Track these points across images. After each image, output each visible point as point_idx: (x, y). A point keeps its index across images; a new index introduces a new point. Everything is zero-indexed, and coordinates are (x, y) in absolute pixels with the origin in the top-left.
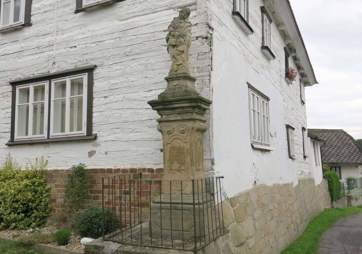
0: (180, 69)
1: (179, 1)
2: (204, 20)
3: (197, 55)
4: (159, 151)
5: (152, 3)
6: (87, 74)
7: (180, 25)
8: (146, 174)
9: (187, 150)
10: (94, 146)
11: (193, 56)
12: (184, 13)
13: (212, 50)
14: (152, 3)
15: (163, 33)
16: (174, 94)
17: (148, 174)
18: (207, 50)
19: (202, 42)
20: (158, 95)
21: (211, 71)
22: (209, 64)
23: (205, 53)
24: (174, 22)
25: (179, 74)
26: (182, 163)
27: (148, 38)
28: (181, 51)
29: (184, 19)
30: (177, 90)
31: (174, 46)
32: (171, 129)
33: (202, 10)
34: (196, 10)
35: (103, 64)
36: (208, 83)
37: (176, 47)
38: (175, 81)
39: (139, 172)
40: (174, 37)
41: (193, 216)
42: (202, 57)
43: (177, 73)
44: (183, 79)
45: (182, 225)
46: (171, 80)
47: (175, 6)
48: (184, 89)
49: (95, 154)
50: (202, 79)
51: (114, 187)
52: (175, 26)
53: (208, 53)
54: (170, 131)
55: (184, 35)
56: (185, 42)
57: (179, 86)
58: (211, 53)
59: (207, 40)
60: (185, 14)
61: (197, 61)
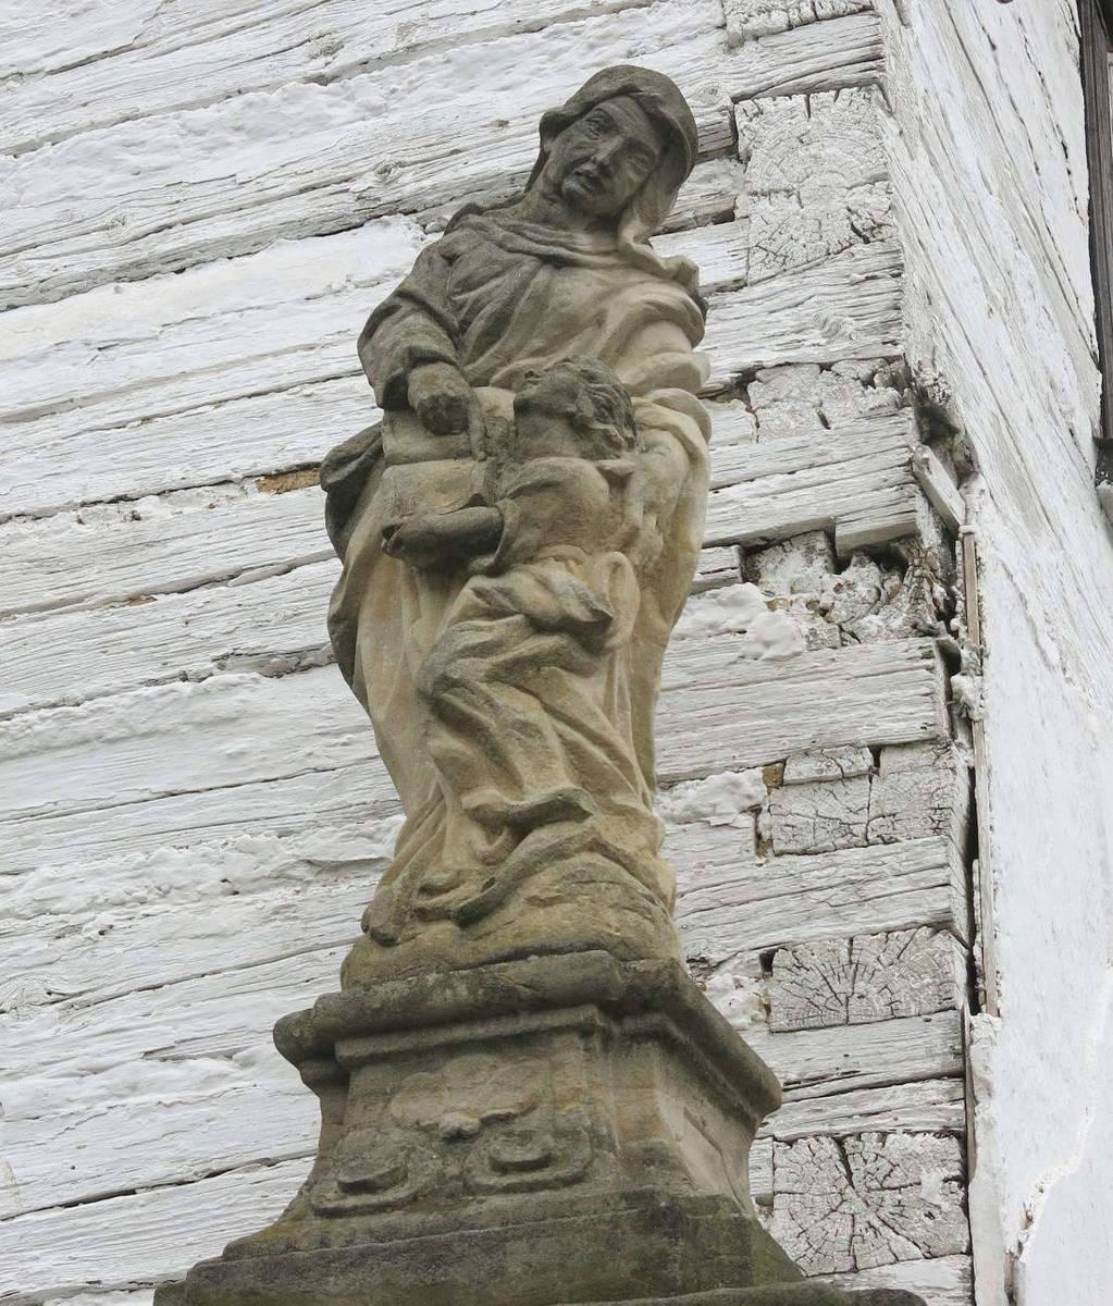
0: (544, 881)
1: (503, 124)
2: (850, 326)
3: (752, 784)
5: (134, 160)
7: (548, 288)
11: (690, 794)
12: (607, 126)
13: (968, 723)
14: (134, 160)
15: (263, 496)
16: (436, 1261)
18: (910, 708)
19: (824, 612)
21: (976, 1010)
22: (938, 902)
23: (877, 750)
24: (451, 259)
25: (520, 954)
27: (47, 565)
28: (566, 625)
29: (608, 224)
30: (498, 1201)
31: (443, 559)
33: (811, 209)
34: (727, 217)
36: (932, 1179)
37: (488, 561)
38: (453, 1069)
40: (459, 441)
42: (833, 805)
43: (490, 947)
44: (585, 1031)
46: (375, 1060)
47: (445, 177)
48: (608, 1178)
50: (843, 1127)
52: (476, 308)
53: (922, 757)
55: (607, 410)
56: (620, 510)
57: (526, 1137)
58: (961, 759)
59: (895, 580)
60: (632, 146)
61: (751, 867)
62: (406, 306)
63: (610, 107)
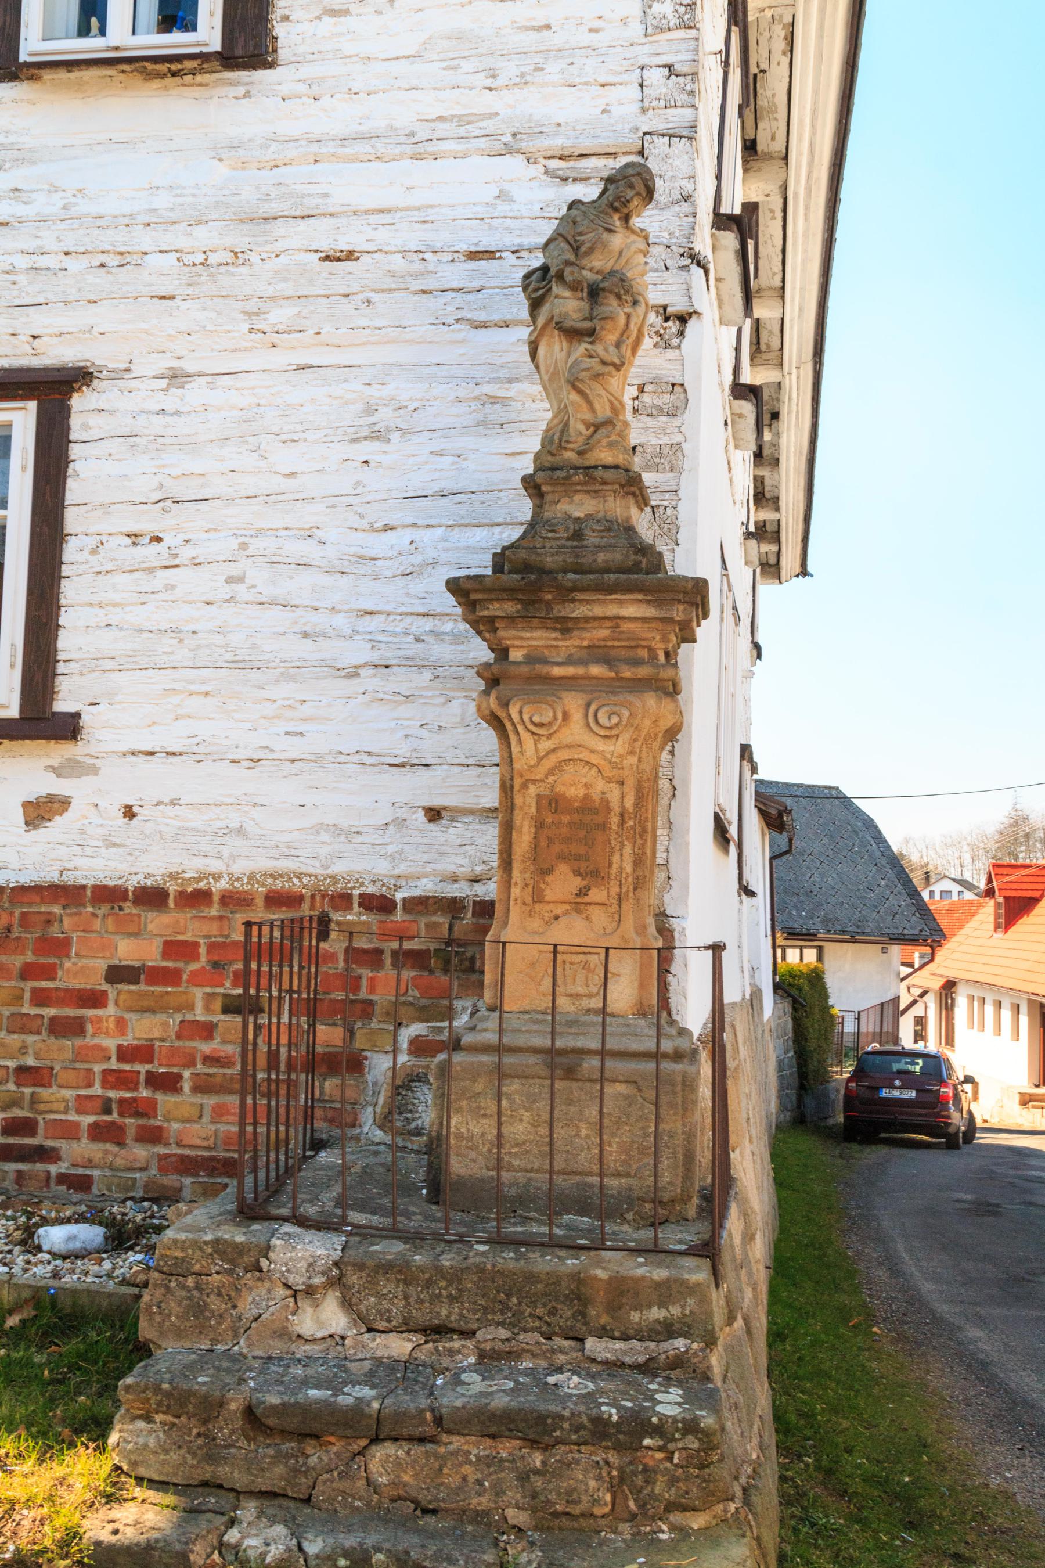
1: (559, 125)
4: (421, 813)
6: (32, 405)
8: (349, 917)
9: (622, 815)
10: (59, 776)
17: (364, 918)
20: (495, 555)
23: (673, 385)
26: (594, 875)
32: (555, 718)
35: (128, 370)
39: (312, 907)
41: (653, 1108)
45: (601, 1151)
49: (66, 815)
51: (253, 980)
54: (550, 724)
62: (561, 239)
63: (633, 179)
